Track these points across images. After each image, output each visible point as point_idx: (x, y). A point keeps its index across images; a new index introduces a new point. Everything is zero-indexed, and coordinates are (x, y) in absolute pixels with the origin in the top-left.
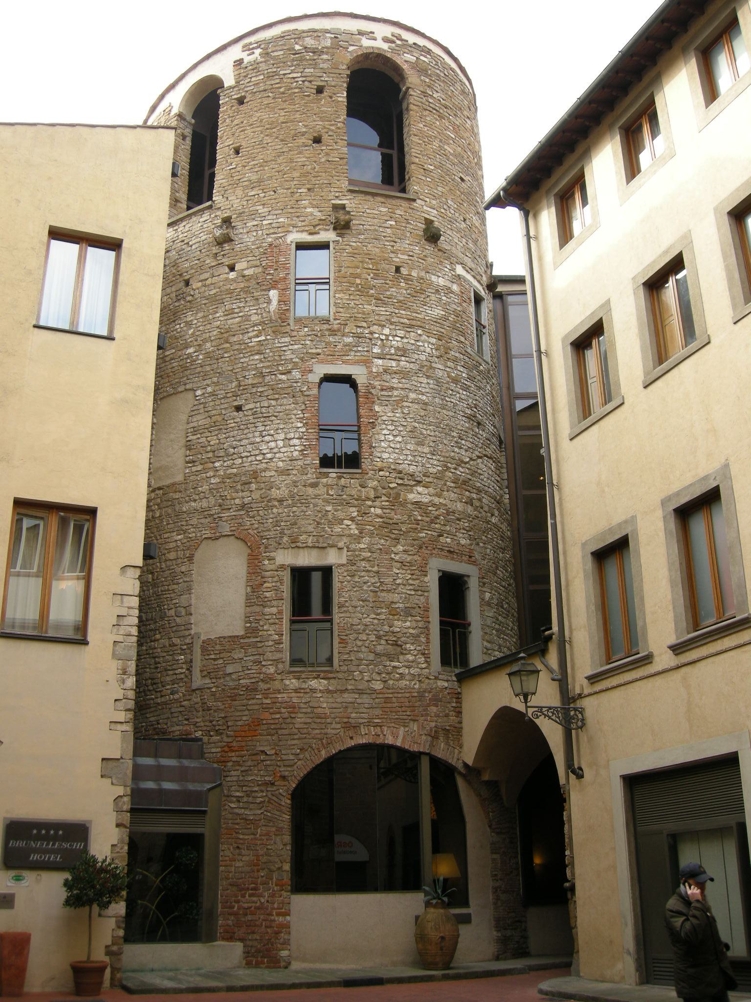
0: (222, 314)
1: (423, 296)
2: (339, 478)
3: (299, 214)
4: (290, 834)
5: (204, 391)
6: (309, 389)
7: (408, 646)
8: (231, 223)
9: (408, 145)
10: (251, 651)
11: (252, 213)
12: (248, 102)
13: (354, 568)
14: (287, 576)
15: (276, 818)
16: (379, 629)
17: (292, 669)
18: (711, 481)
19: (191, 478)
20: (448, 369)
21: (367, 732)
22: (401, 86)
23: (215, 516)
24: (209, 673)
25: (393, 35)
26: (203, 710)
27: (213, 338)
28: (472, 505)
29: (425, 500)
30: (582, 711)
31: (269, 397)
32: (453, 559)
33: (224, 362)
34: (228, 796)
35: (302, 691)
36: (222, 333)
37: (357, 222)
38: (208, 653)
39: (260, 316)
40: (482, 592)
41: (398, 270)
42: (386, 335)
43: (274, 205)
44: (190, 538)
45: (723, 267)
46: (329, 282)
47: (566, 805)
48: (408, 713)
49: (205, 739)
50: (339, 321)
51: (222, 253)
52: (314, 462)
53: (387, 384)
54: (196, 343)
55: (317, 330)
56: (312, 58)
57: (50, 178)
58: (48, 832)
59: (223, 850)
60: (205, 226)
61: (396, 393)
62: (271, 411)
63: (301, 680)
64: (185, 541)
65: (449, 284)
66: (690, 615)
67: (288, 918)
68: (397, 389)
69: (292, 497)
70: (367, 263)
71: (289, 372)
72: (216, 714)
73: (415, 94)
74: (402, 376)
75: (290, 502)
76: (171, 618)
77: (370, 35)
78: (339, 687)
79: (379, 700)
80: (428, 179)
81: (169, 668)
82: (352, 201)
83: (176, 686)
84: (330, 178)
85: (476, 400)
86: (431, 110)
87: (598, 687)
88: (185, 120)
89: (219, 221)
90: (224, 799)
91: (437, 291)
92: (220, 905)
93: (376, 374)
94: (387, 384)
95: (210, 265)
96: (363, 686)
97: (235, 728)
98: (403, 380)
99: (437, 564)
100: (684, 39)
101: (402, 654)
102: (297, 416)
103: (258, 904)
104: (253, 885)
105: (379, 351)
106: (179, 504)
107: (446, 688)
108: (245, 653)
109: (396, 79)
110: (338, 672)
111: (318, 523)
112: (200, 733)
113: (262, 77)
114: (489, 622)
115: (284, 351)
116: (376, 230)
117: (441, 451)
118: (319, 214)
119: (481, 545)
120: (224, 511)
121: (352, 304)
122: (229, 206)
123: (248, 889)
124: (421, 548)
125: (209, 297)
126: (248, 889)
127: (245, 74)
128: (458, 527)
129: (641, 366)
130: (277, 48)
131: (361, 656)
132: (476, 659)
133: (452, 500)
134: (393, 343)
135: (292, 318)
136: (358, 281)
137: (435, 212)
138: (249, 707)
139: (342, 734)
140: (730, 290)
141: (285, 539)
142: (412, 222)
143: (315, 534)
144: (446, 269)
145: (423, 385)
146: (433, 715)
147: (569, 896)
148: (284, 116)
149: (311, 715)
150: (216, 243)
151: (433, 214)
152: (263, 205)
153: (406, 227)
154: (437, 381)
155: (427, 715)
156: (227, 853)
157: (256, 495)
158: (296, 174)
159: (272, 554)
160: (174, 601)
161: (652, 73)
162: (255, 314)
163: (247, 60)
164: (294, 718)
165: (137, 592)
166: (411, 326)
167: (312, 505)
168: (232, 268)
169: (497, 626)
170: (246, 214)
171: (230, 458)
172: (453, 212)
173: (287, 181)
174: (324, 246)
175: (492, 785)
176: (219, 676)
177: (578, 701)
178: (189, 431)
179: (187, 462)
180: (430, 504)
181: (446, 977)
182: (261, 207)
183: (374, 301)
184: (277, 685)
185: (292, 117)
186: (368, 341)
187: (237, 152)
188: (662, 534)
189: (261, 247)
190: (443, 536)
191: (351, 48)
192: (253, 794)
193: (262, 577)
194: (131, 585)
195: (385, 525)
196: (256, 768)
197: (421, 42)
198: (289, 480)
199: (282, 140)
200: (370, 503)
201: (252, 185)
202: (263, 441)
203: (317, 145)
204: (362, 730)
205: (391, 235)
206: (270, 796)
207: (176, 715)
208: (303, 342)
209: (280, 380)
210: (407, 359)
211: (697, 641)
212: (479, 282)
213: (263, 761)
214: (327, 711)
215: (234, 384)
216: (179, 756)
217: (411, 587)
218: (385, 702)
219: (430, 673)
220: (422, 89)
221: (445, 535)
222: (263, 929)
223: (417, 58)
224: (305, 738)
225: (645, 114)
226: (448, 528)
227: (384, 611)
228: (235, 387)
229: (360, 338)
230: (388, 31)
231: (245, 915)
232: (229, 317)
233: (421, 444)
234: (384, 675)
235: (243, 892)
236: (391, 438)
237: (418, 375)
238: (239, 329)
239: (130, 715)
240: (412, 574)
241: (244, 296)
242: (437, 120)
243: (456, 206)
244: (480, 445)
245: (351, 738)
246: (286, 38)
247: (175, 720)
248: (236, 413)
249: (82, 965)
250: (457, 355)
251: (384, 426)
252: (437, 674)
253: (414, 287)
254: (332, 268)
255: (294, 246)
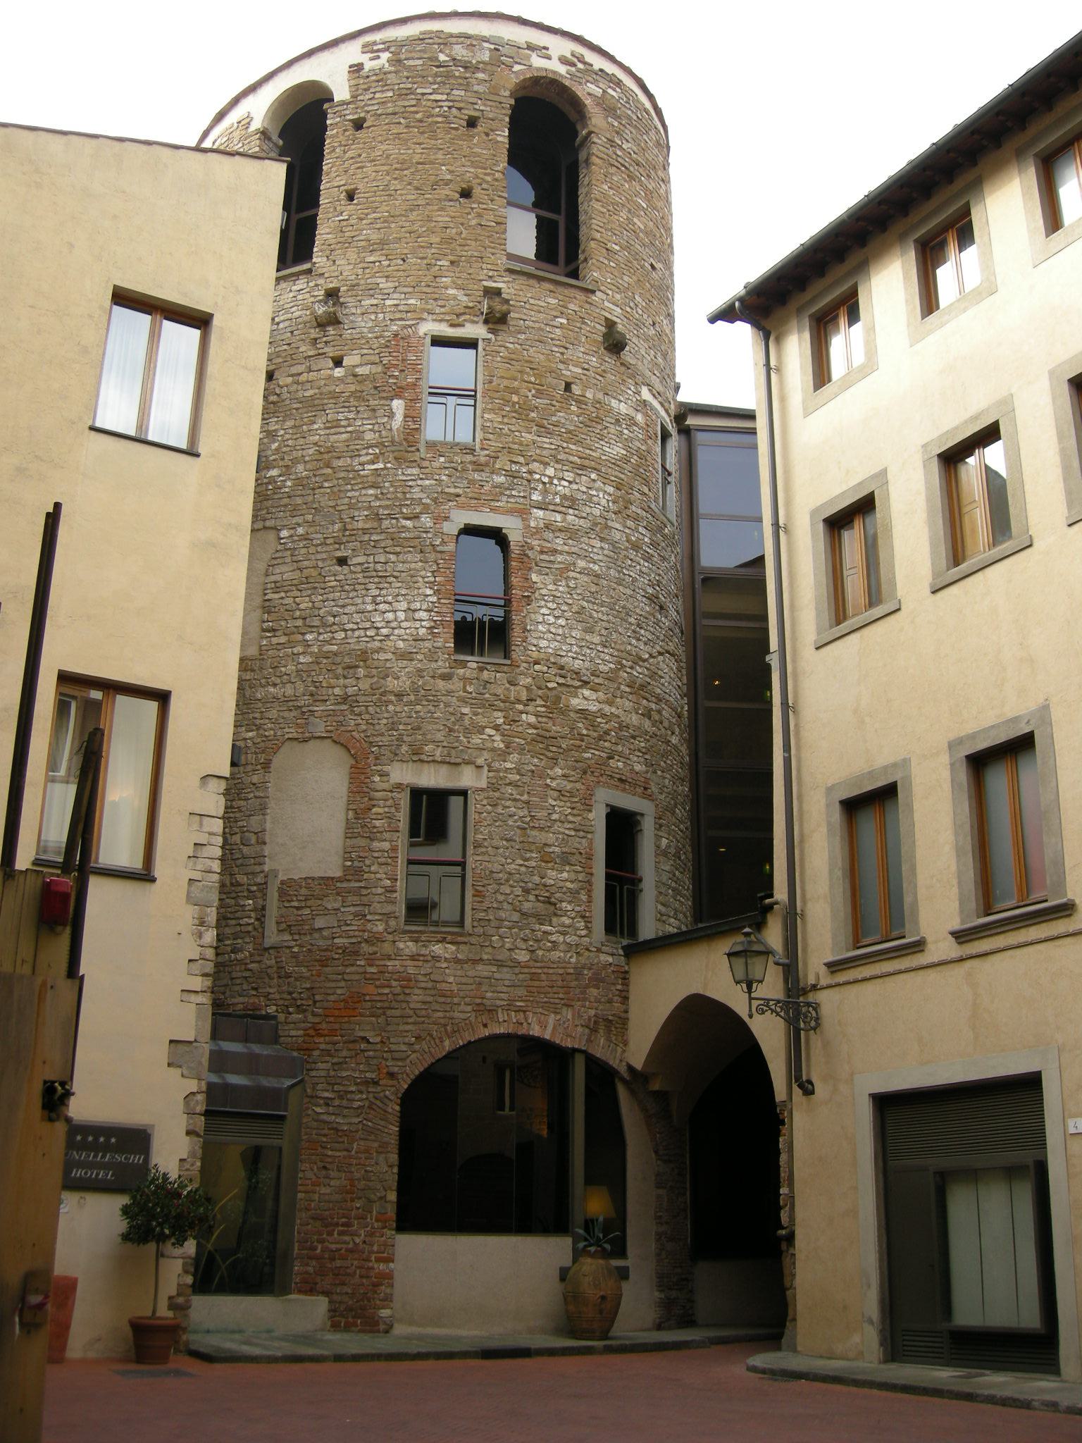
0: (322, 426)
1: (600, 427)
2: (481, 669)
3: (437, 296)
4: (397, 1152)
5: (292, 532)
6: (443, 542)
7: (564, 904)
8: (338, 297)
9: (586, 213)
10: (351, 899)
11: (370, 287)
12: (368, 127)
13: (497, 794)
14: (405, 800)
15: (379, 1130)
16: (526, 880)
17: (408, 928)
18: (1023, 725)
19: (270, 653)
20: (627, 531)
21: (506, 1018)
22: (579, 127)
23: (304, 709)
24: (289, 926)
25: (573, 55)
26: (279, 977)
27: (307, 459)
28: (650, 718)
29: (593, 707)
30: (816, 1007)
31: (387, 550)
32: (624, 790)
33: (324, 494)
34: (312, 1097)
35: (421, 958)
36: (321, 453)
37: (516, 315)
38: (289, 898)
39: (377, 434)
40: (658, 837)
41: (568, 387)
42: (549, 477)
43: (402, 279)
44: (266, 736)
45: (1057, 450)
46: (475, 396)
47: (784, 1129)
48: (561, 996)
49: (281, 1017)
50: (487, 452)
51: (325, 339)
52: (447, 645)
53: (549, 545)
54: (281, 463)
55: (457, 462)
56: (463, 75)
57: (115, 217)
58: (96, 1139)
59: (304, 1171)
60: (300, 297)
61: (560, 558)
62: (389, 569)
63: (420, 944)
64: (259, 740)
65: (632, 412)
66: (980, 893)
67: (392, 1265)
68: (561, 553)
69: (416, 691)
70: (528, 374)
71: (416, 517)
72: (298, 983)
73: (599, 142)
74: (569, 535)
75: (412, 698)
76: (235, 847)
77: (543, 51)
78: (471, 956)
79: (524, 976)
80: (612, 264)
81: (229, 915)
82: (510, 285)
83: (240, 941)
84: (483, 249)
85: (659, 575)
86: (619, 166)
87: (842, 977)
88: (270, 139)
89: (320, 293)
90: (305, 1101)
91: (618, 421)
92: (296, 1245)
93: (534, 530)
94: (549, 545)
95: (305, 354)
96: (503, 955)
97: (326, 1004)
98: (570, 541)
99: (606, 796)
100: (1020, 139)
101: (556, 915)
102: (426, 580)
103: (351, 1246)
104: (344, 1220)
105: (540, 498)
106: (251, 688)
107: (610, 964)
108: (343, 902)
109: (573, 116)
110: (470, 935)
111: (451, 730)
112: (274, 1008)
113: (390, 94)
114: (664, 878)
115: (410, 486)
116: (540, 329)
117: (615, 643)
118: (465, 298)
119: (659, 773)
120: (317, 704)
121: (506, 431)
122: (336, 274)
123: (337, 1224)
124: (585, 773)
125: (303, 399)
126: (337, 1224)
127: (366, 86)
128: (632, 747)
129: (929, 564)
130: (413, 55)
131: (503, 914)
132: (648, 928)
133: (626, 710)
134: (559, 488)
135: (423, 442)
136: (515, 398)
137: (618, 310)
138: (346, 977)
139: (473, 1019)
140: (1065, 480)
141: (404, 748)
142: (589, 322)
143: (445, 744)
144: (629, 392)
145: (595, 550)
146: (592, 999)
147: (784, 1246)
148: (422, 153)
149: (433, 992)
150: (315, 324)
151: (616, 314)
152: (387, 277)
153: (581, 328)
154: (614, 546)
155: (585, 999)
156: (309, 1174)
157: (365, 685)
158: (435, 239)
159: (386, 768)
160: (240, 824)
161: (971, 175)
162: (370, 430)
163: (369, 65)
164: (409, 994)
165: (221, 812)
166: (583, 467)
167: (442, 705)
168: (338, 362)
169: (673, 884)
170: (361, 288)
171: (328, 629)
172: (640, 312)
173: (422, 247)
174: (471, 344)
175: (661, 1096)
176: (303, 932)
177: (811, 995)
178: (269, 586)
179: (264, 630)
180: (599, 714)
181: (609, 1350)
182: (384, 280)
183: (535, 428)
184: (387, 948)
185: (433, 157)
186: (525, 482)
187: (351, 197)
188: (947, 786)
189: (381, 336)
190: (613, 758)
191: (517, 68)
192: (349, 1096)
193: (370, 799)
194: (213, 802)
195: (539, 739)
196: (353, 1060)
197: (610, 68)
198: (411, 667)
199: (417, 189)
200: (520, 707)
201: (372, 247)
202: (376, 610)
203: (466, 200)
204: (500, 1015)
205: (561, 338)
206: (372, 1100)
207: (238, 981)
208: (438, 477)
209: (403, 527)
210: (576, 512)
211: (990, 929)
212: (667, 411)
213: (362, 1051)
214: (454, 987)
215: (337, 527)
216: (246, 1040)
217: (570, 826)
218: (531, 980)
219: (591, 943)
220: (608, 136)
221: (616, 757)
222: (357, 1280)
223: (604, 91)
224: (423, 1022)
225: (952, 227)
226: (620, 748)
227: (534, 855)
228: (339, 530)
229: (515, 477)
230: (567, 47)
231: (332, 1259)
232: (333, 431)
233: (589, 630)
234: (531, 943)
235: (330, 1228)
236: (552, 620)
237: (589, 535)
238: (346, 449)
239: (208, 982)
240: (573, 808)
241: (356, 403)
242: (626, 181)
243: (644, 304)
244: (662, 637)
245: (485, 1026)
246: (427, 41)
247: (237, 988)
248: (339, 568)
249: (147, 1321)
250: (639, 511)
251: (543, 603)
252: (600, 946)
253: (588, 413)
254: (480, 377)
255: (428, 340)
